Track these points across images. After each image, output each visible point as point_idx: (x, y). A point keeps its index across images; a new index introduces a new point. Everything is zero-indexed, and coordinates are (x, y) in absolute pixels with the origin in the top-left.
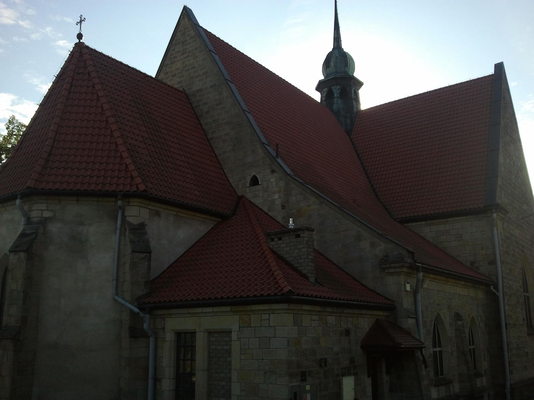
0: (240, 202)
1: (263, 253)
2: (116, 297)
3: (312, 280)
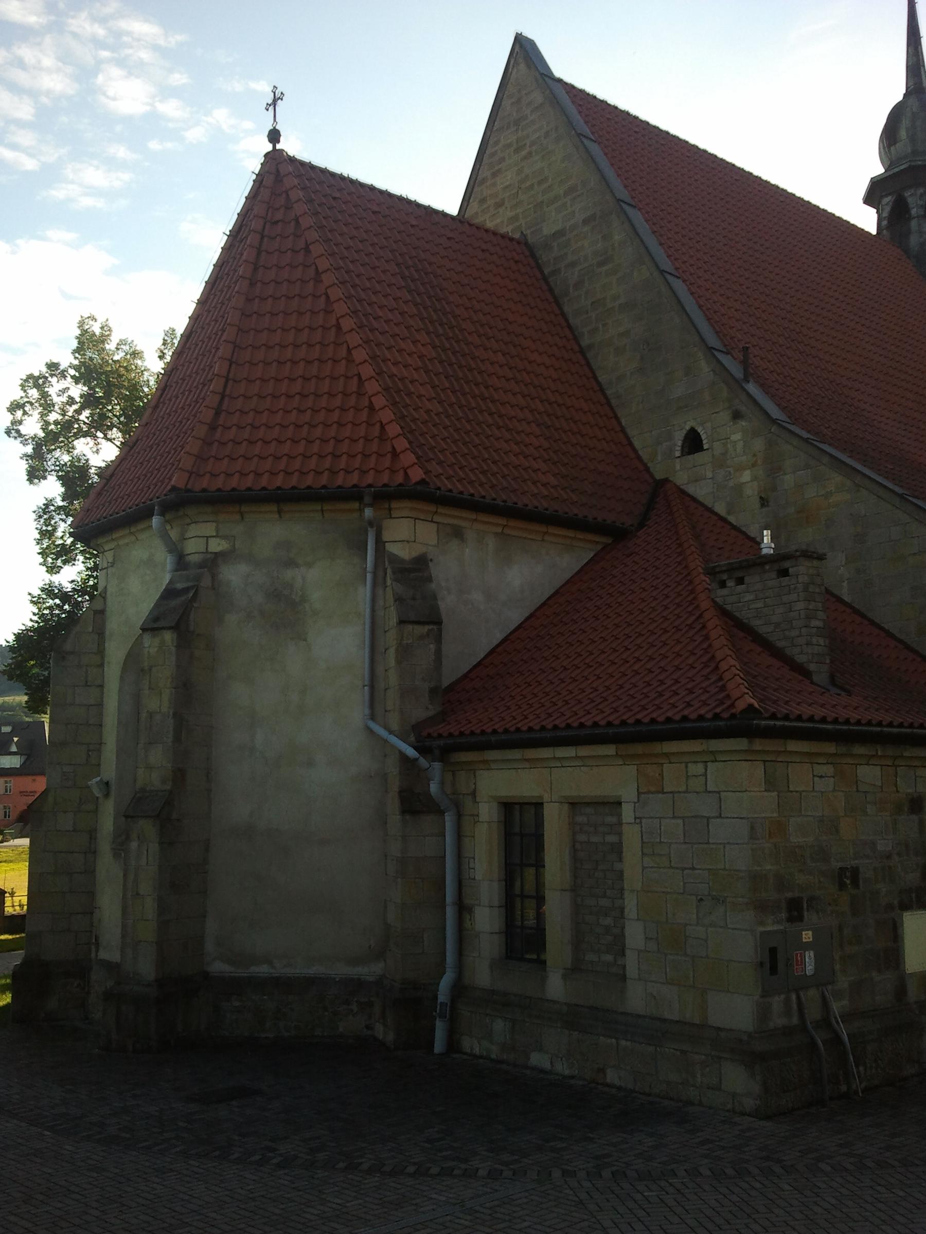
0: (660, 491)
1: (700, 616)
2: (373, 725)
3: (821, 675)
